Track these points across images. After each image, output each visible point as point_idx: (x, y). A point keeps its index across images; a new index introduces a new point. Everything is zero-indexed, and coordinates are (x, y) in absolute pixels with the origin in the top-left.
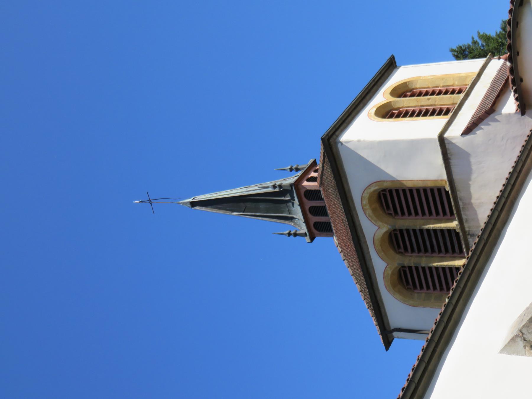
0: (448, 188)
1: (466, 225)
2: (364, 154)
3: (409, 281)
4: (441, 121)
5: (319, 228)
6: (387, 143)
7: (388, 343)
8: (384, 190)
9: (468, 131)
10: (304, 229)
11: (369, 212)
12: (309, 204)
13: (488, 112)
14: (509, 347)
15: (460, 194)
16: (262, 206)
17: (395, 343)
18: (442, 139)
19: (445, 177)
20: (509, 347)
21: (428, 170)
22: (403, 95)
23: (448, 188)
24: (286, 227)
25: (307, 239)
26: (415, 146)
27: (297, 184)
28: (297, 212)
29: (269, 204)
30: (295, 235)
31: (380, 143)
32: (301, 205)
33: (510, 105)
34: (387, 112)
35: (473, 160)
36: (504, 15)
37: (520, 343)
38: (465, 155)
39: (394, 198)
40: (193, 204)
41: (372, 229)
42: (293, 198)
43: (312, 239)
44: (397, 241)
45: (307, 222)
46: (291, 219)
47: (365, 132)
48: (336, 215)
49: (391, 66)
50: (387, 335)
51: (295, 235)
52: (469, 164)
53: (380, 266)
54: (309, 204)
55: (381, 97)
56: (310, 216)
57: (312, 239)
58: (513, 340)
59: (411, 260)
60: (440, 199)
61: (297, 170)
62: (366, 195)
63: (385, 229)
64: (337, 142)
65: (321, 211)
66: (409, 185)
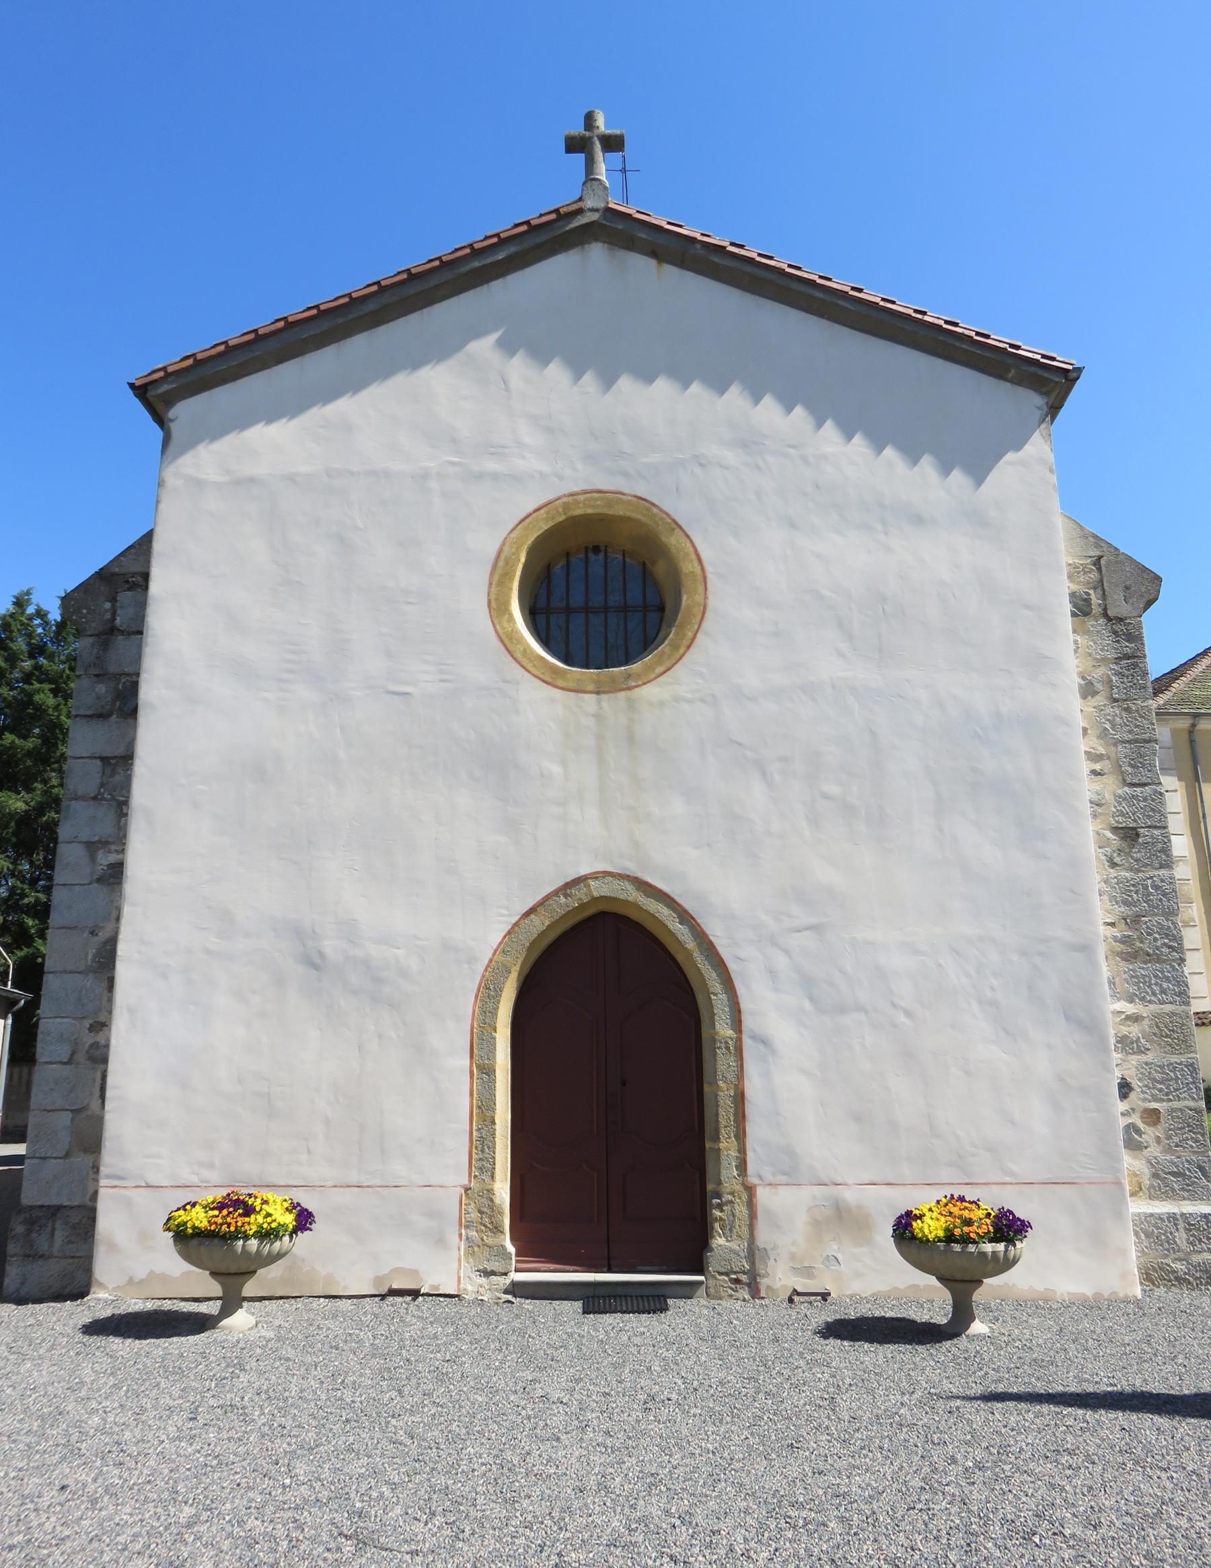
14: (1079, 370)
20: (1079, 370)
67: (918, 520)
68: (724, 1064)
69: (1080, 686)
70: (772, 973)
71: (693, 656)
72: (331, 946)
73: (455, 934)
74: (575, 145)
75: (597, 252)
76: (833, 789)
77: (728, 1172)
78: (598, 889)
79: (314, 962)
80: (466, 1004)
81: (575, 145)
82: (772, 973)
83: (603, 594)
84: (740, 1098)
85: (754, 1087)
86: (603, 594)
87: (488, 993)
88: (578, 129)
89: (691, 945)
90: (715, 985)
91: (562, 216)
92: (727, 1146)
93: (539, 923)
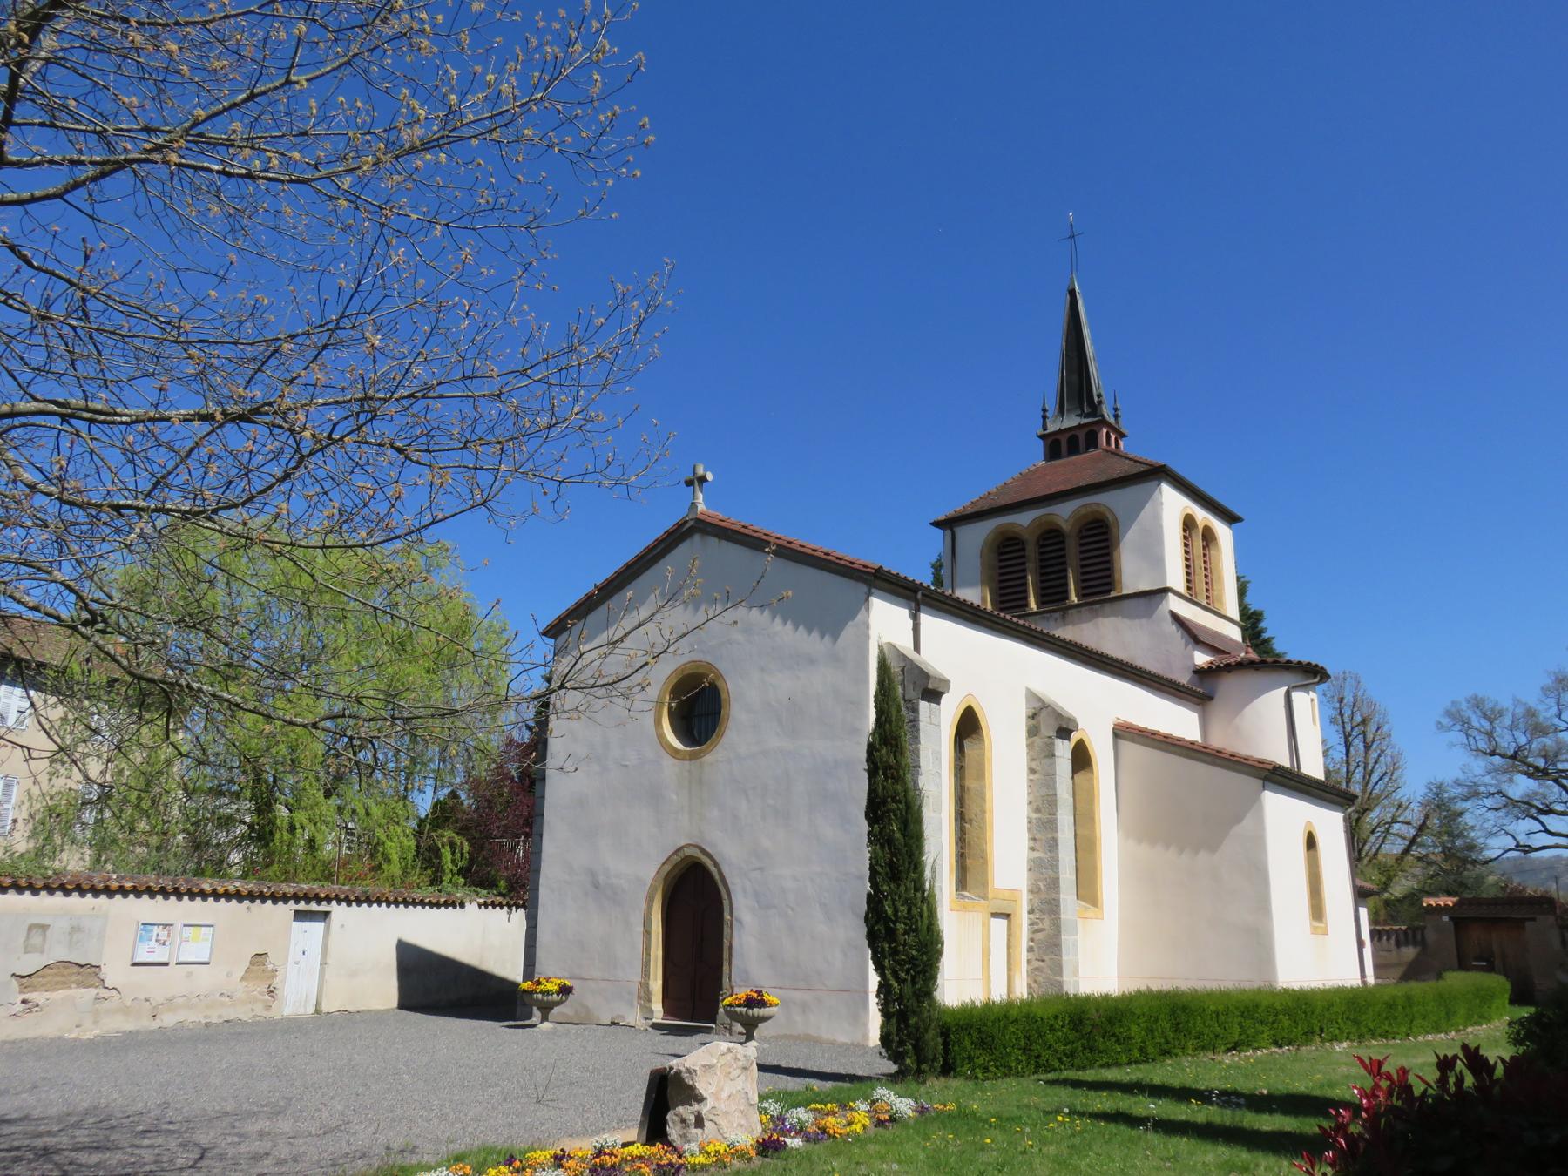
0: (1113, 594)
1: (1073, 611)
2: (1148, 508)
3: (1007, 550)
4: (1181, 587)
5: (1056, 446)
6: (1161, 533)
7: (937, 524)
8: (1107, 526)
9: (1175, 617)
10: (1052, 428)
11: (1083, 511)
12: (1081, 435)
13: (1193, 635)
14: (1032, 696)
15: (1108, 607)
16: (1075, 378)
17: (939, 532)
18: (1166, 590)
19: (1125, 592)
20: (1032, 696)
21: (1132, 575)
22: (1204, 537)
23: (1113, 594)
24: (1052, 406)
25: (1040, 431)
26: (1158, 562)
27: (1103, 422)
28: (1072, 421)
29: (1076, 383)
30: (1044, 418)
31: (1161, 527)
32: (1080, 426)
33: (1202, 659)
34: (1189, 523)
35: (1144, 621)
36: (1294, 656)
37: (1038, 705)
38: (1149, 614)
39: (1099, 539)
40: (1072, 293)
41: (1065, 513)
42: (1087, 416)
43: (1041, 437)
44: (1051, 536)
45: (1061, 431)
46: (1061, 411)
47: (1172, 504)
48: (1078, 469)
49: (1230, 518)
50: (949, 524)
51: (1044, 418)
52: (1139, 617)
53: (1024, 519)
54: (1081, 435)
55: (1202, 516)
56: (1068, 435)
57: (1041, 437)
58: (1040, 699)
59: (1032, 552)
60: (1100, 586)
61: (1116, 417)
62: (1102, 509)
63: (1065, 527)
64: (1160, 480)
65: (1074, 449)
66: (1115, 554)
67: (812, 661)
68: (726, 930)
69: (869, 895)
70: (744, 890)
71: (724, 740)
72: (601, 879)
73: (641, 871)
74: (689, 483)
75: (697, 537)
76: (771, 802)
77: (725, 979)
78: (688, 852)
79: (596, 886)
80: (643, 904)
81: (689, 483)
82: (744, 890)
83: (698, 709)
84: (730, 947)
85: (735, 943)
86: (698, 709)
87: (650, 900)
88: (689, 476)
89: (717, 877)
90: (725, 896)
91: (679, 526)
92: (726, 968)
93: (668, 868)
